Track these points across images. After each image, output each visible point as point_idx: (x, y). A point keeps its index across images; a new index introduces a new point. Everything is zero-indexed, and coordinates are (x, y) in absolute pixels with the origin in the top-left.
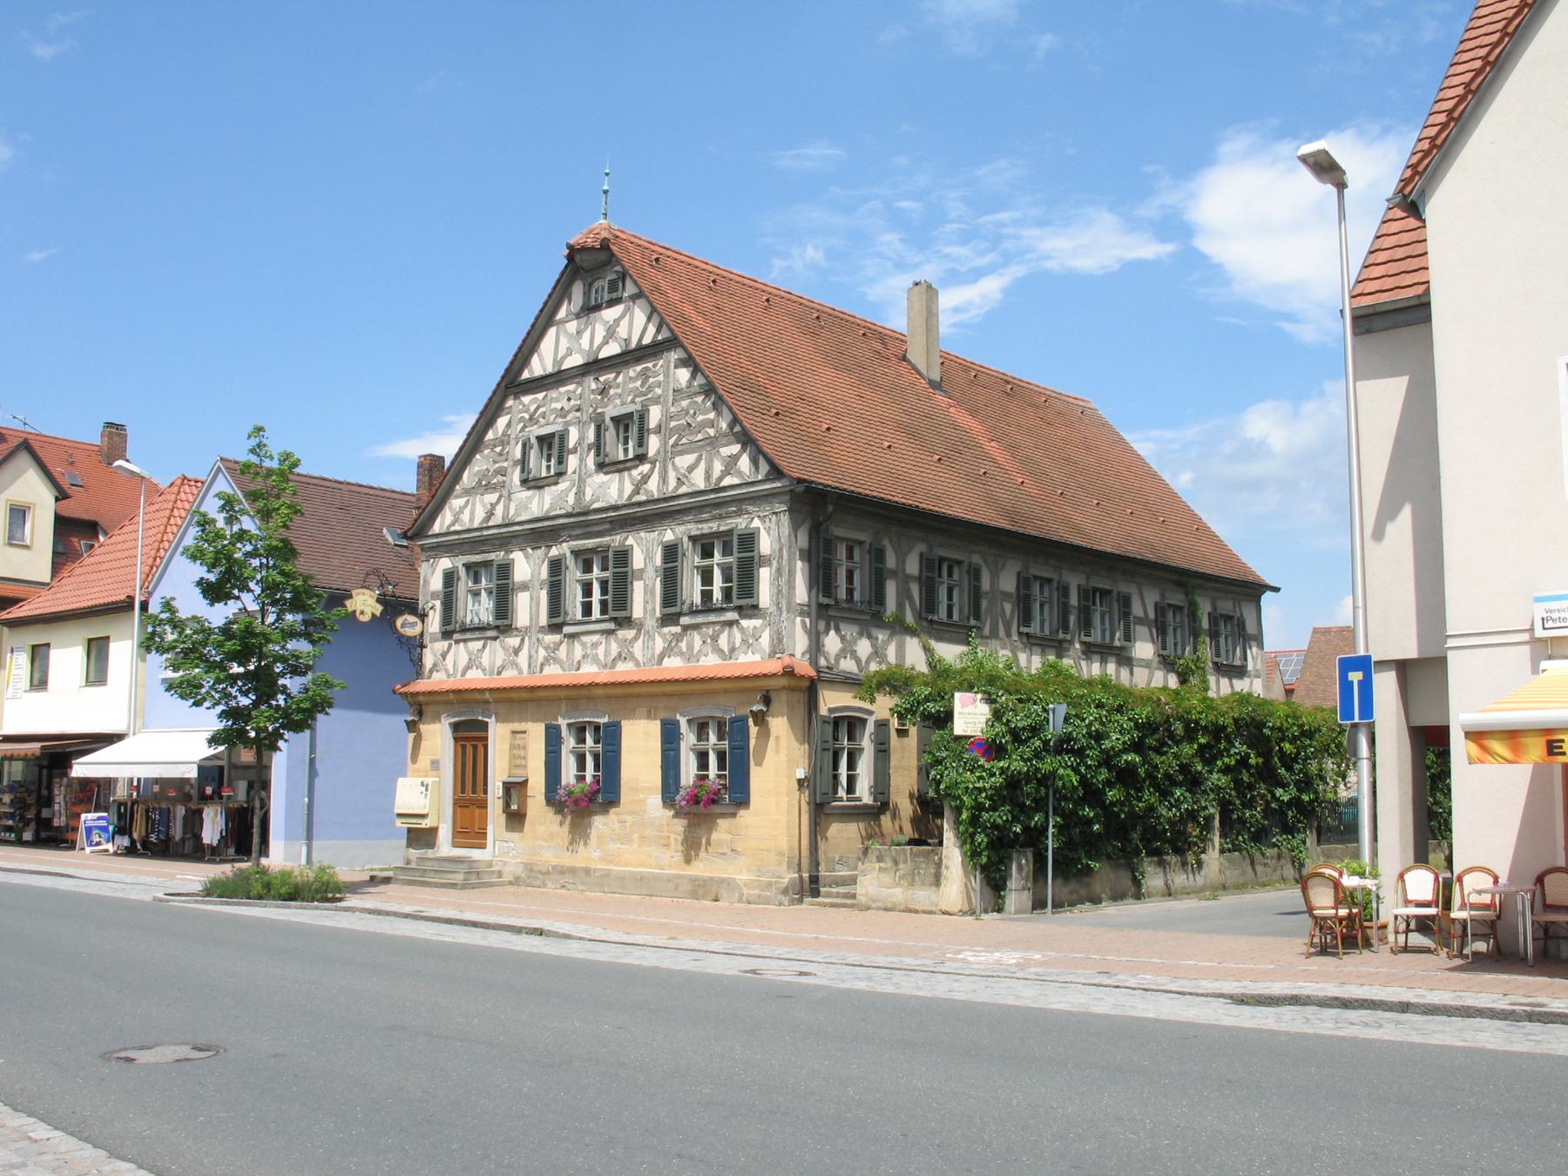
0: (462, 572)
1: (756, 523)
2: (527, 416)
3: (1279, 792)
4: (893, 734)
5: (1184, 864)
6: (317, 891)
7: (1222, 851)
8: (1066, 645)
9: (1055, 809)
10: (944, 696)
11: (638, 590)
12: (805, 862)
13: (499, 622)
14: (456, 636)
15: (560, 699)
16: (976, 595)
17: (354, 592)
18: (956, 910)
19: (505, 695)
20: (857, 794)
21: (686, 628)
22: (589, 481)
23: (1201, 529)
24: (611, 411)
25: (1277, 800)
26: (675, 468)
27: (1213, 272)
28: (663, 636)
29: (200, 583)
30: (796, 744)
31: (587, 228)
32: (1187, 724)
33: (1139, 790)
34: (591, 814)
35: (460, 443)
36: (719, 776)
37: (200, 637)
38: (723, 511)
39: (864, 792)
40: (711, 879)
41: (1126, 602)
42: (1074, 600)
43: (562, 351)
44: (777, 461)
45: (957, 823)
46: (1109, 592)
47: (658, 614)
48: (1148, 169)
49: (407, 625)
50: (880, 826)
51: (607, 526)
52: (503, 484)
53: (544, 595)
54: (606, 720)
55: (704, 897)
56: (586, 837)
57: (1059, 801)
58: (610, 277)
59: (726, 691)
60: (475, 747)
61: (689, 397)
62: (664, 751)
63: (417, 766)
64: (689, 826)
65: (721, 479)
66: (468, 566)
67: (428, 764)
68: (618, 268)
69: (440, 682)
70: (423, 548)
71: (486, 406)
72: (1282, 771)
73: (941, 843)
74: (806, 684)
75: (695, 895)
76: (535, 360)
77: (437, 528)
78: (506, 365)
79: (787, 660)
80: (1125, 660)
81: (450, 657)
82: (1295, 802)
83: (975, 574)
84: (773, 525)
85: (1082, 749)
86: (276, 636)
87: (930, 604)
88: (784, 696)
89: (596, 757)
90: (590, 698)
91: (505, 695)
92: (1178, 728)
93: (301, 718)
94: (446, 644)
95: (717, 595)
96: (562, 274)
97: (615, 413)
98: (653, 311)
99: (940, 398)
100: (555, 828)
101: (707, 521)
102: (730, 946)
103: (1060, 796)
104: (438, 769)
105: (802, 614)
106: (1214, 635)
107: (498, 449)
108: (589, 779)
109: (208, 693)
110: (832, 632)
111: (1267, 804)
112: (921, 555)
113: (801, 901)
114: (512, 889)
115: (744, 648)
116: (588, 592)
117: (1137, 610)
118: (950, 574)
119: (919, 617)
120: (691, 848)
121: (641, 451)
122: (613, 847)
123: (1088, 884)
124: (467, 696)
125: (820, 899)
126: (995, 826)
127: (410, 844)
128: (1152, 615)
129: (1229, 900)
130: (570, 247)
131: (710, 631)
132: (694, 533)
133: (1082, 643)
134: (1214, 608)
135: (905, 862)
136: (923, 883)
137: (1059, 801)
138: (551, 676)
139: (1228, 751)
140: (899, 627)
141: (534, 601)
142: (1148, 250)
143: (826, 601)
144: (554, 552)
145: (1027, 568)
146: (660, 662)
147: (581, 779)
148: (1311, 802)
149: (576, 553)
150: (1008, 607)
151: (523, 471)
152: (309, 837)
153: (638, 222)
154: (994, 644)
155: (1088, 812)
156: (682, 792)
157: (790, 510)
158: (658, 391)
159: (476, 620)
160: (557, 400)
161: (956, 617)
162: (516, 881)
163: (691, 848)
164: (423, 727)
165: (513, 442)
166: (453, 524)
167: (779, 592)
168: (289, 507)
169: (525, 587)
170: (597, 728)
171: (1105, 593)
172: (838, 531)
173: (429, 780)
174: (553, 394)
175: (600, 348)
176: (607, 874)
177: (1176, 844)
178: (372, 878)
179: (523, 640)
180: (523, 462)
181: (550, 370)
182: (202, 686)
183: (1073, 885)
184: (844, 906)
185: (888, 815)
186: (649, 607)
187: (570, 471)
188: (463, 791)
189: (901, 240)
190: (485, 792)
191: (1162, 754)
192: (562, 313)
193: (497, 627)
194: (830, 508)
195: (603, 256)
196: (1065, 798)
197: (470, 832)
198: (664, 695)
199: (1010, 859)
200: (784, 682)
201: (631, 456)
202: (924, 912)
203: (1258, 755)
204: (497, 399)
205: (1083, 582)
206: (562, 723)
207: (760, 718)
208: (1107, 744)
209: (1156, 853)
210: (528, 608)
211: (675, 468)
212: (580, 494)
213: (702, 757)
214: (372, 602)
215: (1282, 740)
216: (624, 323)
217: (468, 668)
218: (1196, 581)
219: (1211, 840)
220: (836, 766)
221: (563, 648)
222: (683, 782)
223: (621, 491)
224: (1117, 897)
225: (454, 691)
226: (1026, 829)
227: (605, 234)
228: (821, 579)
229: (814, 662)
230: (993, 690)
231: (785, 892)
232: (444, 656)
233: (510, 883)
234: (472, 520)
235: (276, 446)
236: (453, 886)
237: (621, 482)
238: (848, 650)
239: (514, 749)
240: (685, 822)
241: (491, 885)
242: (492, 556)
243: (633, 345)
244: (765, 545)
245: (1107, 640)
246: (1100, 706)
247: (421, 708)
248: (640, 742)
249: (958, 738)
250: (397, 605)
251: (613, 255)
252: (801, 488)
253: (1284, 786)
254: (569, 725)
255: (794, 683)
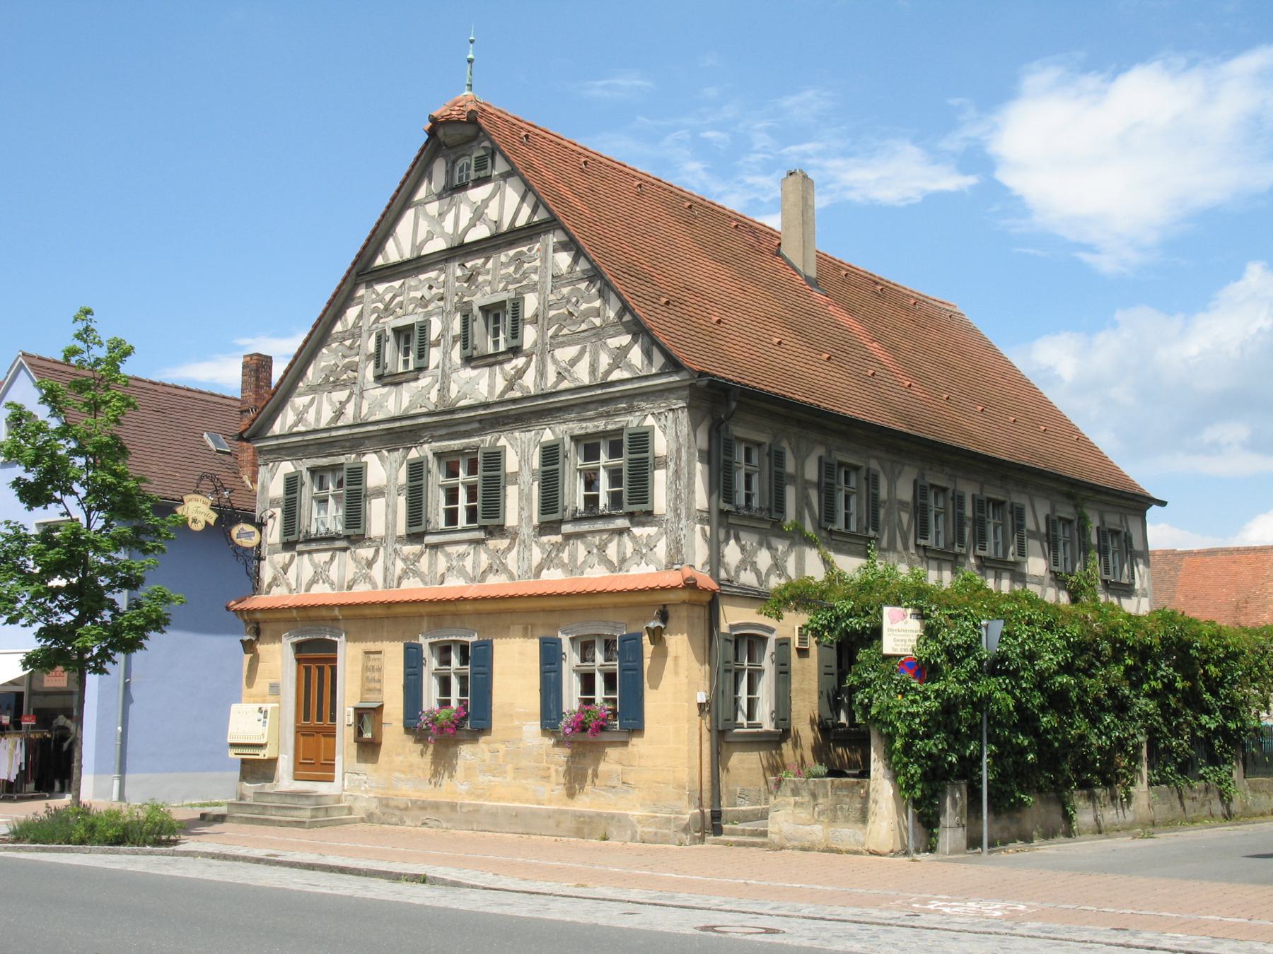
0: (306, 477)
1: (650, 421)
2: (381, 306)
3: (1204, 719)
4: (794, 653)
5: (1113, 798)
6: (149, 833)
7: (1150, 784)
8: (961, 559)
9: (989, 736)
10: (871, 611)
11: (512, 496)
12: (707, 796)
13: (350, 532)
14: (300, 547)
15: (421, 616)
16: (874, 503)
17: (186, 498)
18: (886, 850)
19: (357, 612)
20: (757, 720)
21: (568, 537)
22: (454, 376)
23: (1082, 441)
24: (479, 300)
25: (1201, 727)
26: (555, 361)
27: (1013, 204)
28: (542, 546)
29: (16, 483)
30: (696, 665)
31: (450, 99)
32: (1113, 641)
33: (1070, 716)
34: (457, 742)
35: (300, 343)
36: (606, 700)
37: (14, 545)
38: (611, 408)
39: (765, 718)
40: (599, 815)
41: (1019, 514)
42: (968, 512)
43: (422, 235)
44: (675, 352)
45: (888, 754)
46: (1003, 503)
47: (535, 522)
48: (954, 102)
49: (243, 535)
50: (781, 755)
51: (476, 425)
52: (354, 382)
53: (402, 503)
54: (475, 638)
55: (590, 836)
56: (451, 769)
57: (993, 727)
58: (476, 154)
59: (616, 607)
60: (321, 670)
61: (571, 283)
62: (544, 674)
63: (253, 690)
64: (572, 756)
65: (608, 372)
66: (313, 471)
67: (267, 689)
68: (486, 144)
69: (281, 597)
70: (260, 451)
71: (335, 296)
72: (1207, 696)
73: (865, 773)
74: (708, 598)
75: (579, 833)
76: (390, 245)
77: (277, 428)
78: (358, 250)
79: (688, 573)
80: (1019, 576)
81: (292, 571)
82: (1222, 731)
83: (873, 480)
84: (669, 423)
85: (1017, 670)
86: (106, 543)
87: (829, 513)
88: (683, 612)
89: (463, 679)
90: (456, 614)
91: (357, 612)
92: (1106, 646)
93: (126, 639)
94: (287, 555)
95: (604, 500)
96: (422, 150)
97: (484, 302)
98: (528, 189)
99: (817, 294)
100: (415, 758)
101: (591, 419)
102: (652, 895)
103: (995, 722)
104: (277, 693)
105: (701, 521)
106: (1103, 551)
107: (348, 343)
108: (454, 704)
109: (24, 607)
110: (732, 542)
111: (1193, 732)
112: (820, 459)
113: (702, 840)
114: (367, 826)
115: (637, 558)
116: (452, 496)
117: (1030, 524)
118: (847, 482)
119: (819, 527)
120: (575, 780)
121: (514, 343)
122: (483, 779)
123: (1019, 821)
124: (313, 613)
125: (723, 838)
126: (930, 756)
127: (244, 777)
128: (1043, 529)
129: (1165, 839)
130: (433, 120)
131: (597, 540)
132: (577, 432)
133: (977, 557)
134: (1103, 522)
135: (826, 795)
136: (847, 819)
137: (993, 727)
138: (412, 591)
139: (1154, 673)
140: (798, 538)
141: (391, 509)
142: (951, 182)
143: (727, 507)
144: (414, 454)
145: (923, 476)
146: (538, 574)
147: (445, 704)
148: (1239, 729)
149: (439, 456)
150: (905, 517)
151: (377, 366)
152: (122, 770)
153: (508, 97)
154: (892, 557)
155: (1023, 740)
156: (567, 719)
157: (689, 407)
158: (535, 277)
159: (322, 530)
160: (416, 289)
161: (853, 528)
162: (369, 818)
163: (575, 780)
164: (261, 648)
165: (365, 335)
166: (296, 425)
167: (678, 497)
168: (121, 399)
169: (379, 493)
170: (464, 649)
171: (998, 504)
172: (738, 431)
173: (267, 706)
174: (412, 282)
175: (466, 231)
176: (476, 810)
177: (1103, 775)
178: (203, 816)
179: (377, 551)
180: (378, 356)
181: (407, 255)
182: (16, 601)
183: (1004, 821)
184: (753, 845)
185: (790, 742)
186: (525, 514)
187: (432, 365)
188: (307, 718)
189: (705, 170)
190: (333, 719)
191: (1092, 676)
192: (421, 194)
193: (347, 537)
194: (734, 405)
195: (469, 131)
196: (1000, 724)
197: (314, 762)
198: (543, 610)
199: (944, 792)
200: (684, 595)
201: (502, 348)
202: (848, 852)
203: (1185, 678)
204: (346, 288)
205: (977, 492)
206: (424, 641)
207: (657, 636)
208: (1040, 664)
209: (1085, 785)
210: (383, 516)
211: (555, 361)
212: (444, 390)
213: (587, 682)
214: (205, 509)
215: (1207, 662)
216: (494, 204)
217: (313, 582)
218: (1085, 493)
219: (1139, 771)
220: (736, 691)
221: (425, 560)
222: (566, 707)
223: (491, 387)
224: (1049, 834)
225: (297, 608)
226: (962, 758)
227: (471, 106)
228: (721, 483)
229: (714, 574)
230: (925, 604)
231: (686, 829)
232: (285, 569)
233: (363, 820)
234: (318, 419)
235: (106, 330)
236: (300, 824)
237: (492, 378)
238: (748, 562)
239: (368, 672)
240: (567, 751)
241: (342, 822)
242: (342, 459)
243: (505, 228)
244: (661, 445)
245: (1000, 555)
246: (1030, 623)
247: (257, 627)
248: (515, 665)
249: (887, 658)
250: (228, 516)
251: (480, 129)
252: (703, 382)
253: (1209, 712)
254: (431, 644)
255: (695, 597)
